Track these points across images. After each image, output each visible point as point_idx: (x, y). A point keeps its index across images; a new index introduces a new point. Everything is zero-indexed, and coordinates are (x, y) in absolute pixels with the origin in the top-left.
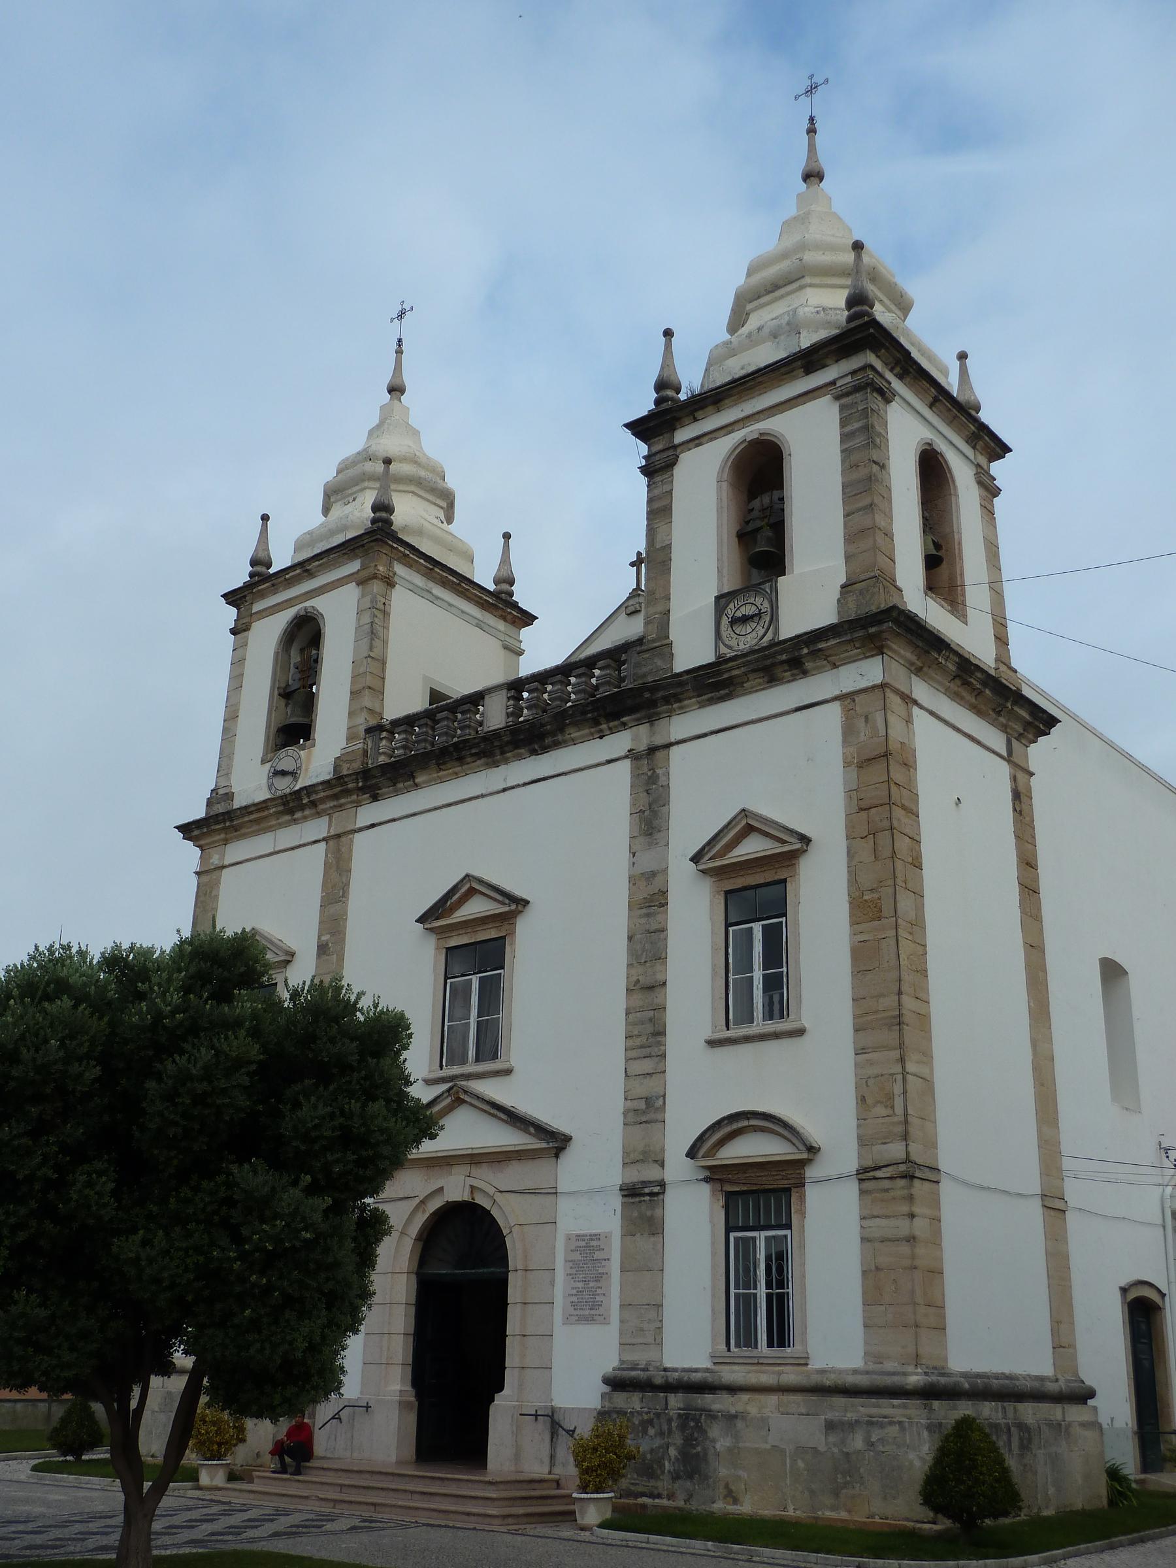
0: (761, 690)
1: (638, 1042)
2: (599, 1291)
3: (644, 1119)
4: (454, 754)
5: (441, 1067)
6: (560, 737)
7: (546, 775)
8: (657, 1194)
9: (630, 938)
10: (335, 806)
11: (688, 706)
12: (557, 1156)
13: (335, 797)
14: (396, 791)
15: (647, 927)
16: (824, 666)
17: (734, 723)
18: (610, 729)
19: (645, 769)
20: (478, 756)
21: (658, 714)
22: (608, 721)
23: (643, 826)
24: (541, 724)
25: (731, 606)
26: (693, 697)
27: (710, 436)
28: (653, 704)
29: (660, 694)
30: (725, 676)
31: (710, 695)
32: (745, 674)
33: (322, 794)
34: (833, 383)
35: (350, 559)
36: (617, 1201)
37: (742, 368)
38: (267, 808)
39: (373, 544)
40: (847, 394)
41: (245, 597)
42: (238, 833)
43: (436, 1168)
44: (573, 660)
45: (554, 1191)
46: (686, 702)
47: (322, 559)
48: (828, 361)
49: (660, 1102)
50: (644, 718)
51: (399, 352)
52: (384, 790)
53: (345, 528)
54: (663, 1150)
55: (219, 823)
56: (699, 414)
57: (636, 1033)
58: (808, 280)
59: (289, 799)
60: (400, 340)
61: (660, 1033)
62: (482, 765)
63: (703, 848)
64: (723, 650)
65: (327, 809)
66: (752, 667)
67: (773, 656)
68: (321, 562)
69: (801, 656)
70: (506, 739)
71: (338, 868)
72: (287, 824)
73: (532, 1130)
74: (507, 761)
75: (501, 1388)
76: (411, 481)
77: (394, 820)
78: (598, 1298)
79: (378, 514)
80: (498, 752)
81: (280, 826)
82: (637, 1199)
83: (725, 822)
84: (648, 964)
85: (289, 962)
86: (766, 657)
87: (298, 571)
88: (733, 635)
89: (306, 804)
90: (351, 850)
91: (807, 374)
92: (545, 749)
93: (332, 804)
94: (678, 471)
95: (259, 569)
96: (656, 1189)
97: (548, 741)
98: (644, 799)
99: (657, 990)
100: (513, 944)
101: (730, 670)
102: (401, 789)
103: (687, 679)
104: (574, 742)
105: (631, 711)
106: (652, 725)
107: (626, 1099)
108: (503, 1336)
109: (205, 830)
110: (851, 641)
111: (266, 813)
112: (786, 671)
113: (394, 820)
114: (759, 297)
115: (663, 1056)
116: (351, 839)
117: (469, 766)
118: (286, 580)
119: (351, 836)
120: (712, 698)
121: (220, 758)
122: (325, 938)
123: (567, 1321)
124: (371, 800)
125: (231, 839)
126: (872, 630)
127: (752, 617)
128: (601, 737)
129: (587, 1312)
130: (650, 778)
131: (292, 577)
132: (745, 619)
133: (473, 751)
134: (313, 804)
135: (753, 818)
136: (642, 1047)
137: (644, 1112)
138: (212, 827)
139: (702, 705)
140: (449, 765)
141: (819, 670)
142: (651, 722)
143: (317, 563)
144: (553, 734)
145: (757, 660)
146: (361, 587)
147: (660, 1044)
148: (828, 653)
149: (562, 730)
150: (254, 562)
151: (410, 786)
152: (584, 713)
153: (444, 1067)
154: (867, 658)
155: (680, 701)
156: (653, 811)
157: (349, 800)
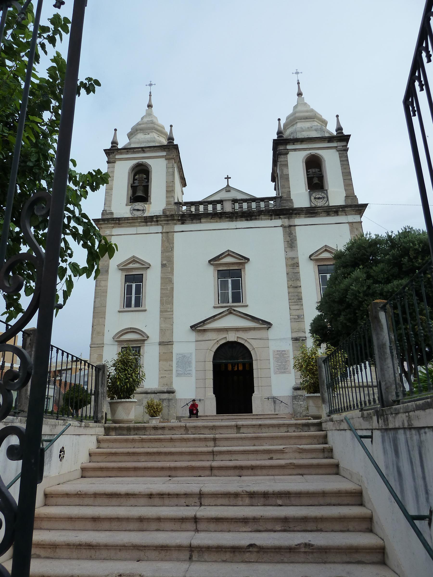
0: (324, 217)
1: (293, 301)
2: (286, 365)
3: (297, 321)
4: (219, 215)
5: (219, 303)
6: (258, 217)
7: (252, 227)
8: (304, 340)
9: (287, 274)
10: (166, 223)
11: (301, 217)
12: (268, 329)
13: (168, 220)
14: (192, 223)
15: (293, 271)
16: (343, 214)
17: (315, 224)
18: (275, 218)
19: (288, 231)
20: (227, 217)
21: (292, 217)
22: (275, 216)
23: (289, 245)
24: (253, 212)
25: (314, 194)
26: (304, 215)
27: (299, 150)
28: (292, 214)
29: (295, 212)
30: (316, 211)
31: (309, 215)
32: (322, 212)
33: (163, 219)
34: (337, 147)
35: (161, 151)
36: (291, 342)
37: (307, 135)
38: (137, 219)
39: (173, 149)
40: (341, 151)
41: (114, 152)
42: (120, 225)
43: (221, 332)
44: (205, 200)
45: (268, 339)
46: (301, 216)
47: (151, 148)
48: (335, 141)
49: (303, 316)
50: (287, 217)
51: (150, 95)
52: (187, 222)
53: (154, 141)
54: (305, 329)
55: (113, 221)
56: (295, 143)
57: (292, 298)
58: (315, 120)
59: (148, 218)
60: (150, 92)
61: (300, 299)
62: (227, 221)
63: (314, 253)
64: (313, 205)
65: (162, 224)
66: (324, 210)
67: (331, 209)
68: (150, 149)
69: (339, 211)
70: (239, 214)
71: (168, 242)
72: (143, 226)
73: (261, 322)
74: (236, 221)
75: (254, 392)
76: (165, 134)
77: (192, 231)
78: (286, 367)
79: (169, 141)
80: (234, 218)
81: (140, 226)
82: (298, 341)
83: (320, 248)
84: (294, 281)
85: (149, 268)
86: (329, 209)
87: (140, 150)
88: (315, 201)
89: (154, 221)
90: (174, 237)
91: (328, 143)
92: (251, 220)
93: (165, 222)
94: (288, 155)
95: (114, 145)
96: (304, 339)
97: (253, 218)
98: (288, 239)
99: (298, 288)
100: (244, 271)
101: (318, 210)
102: (194, 222)
103: (304, 210)
104: (262, 219)
105: (284, 214)
106: (289, 220)
107: (290, 315)
108: (253, 378)
109: (106, 222)
110: (354, 210)
111: (136, 221)
112: (333, 213)
113: (192, 231)
114: (301, 119)
115: (302, 305)
116: (173, 234)
117: (223, 220)
118: (133, 151)
119: (173, 233)
120: (309, 216)
121: (105, 201)
122: (165, 262)
123: (275, 373)
124: (181, 224)
125: (116, 227)
126: (360, 208)
127: (322, 198)
128: (271, 220)
129: (283, 371)
130: (290, 233)
131: (136, 151)
132: (319, 198)
133: (227, 216)
134: (157, 221)
135: (328, 248)
136: (295, 302)
137: (297, 319)
138: (110, 222)
139: (305, 217)
140: (215, 218)
141: (342, 215)
142: (289, 219)
143: (149, 149)
144: (256, 216)
145: (326, 209)
146: (167, 160)
147: (300, 302)
148: (346, 211)
149: (259, 215)
150: (112, 143)
151: (199, 222)
152: (269, 212)
153: (220, 304)
154: (355, 215)
155: (300, 215)
156: (292, 242)
157: (173, 222)
